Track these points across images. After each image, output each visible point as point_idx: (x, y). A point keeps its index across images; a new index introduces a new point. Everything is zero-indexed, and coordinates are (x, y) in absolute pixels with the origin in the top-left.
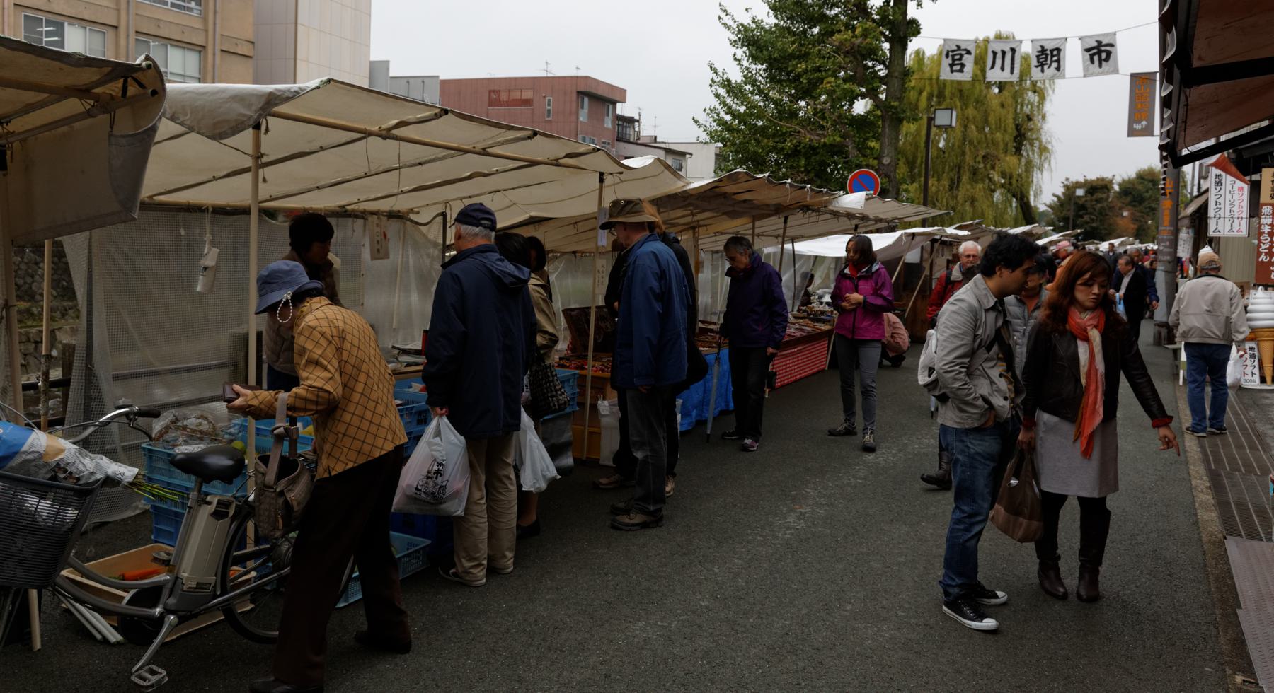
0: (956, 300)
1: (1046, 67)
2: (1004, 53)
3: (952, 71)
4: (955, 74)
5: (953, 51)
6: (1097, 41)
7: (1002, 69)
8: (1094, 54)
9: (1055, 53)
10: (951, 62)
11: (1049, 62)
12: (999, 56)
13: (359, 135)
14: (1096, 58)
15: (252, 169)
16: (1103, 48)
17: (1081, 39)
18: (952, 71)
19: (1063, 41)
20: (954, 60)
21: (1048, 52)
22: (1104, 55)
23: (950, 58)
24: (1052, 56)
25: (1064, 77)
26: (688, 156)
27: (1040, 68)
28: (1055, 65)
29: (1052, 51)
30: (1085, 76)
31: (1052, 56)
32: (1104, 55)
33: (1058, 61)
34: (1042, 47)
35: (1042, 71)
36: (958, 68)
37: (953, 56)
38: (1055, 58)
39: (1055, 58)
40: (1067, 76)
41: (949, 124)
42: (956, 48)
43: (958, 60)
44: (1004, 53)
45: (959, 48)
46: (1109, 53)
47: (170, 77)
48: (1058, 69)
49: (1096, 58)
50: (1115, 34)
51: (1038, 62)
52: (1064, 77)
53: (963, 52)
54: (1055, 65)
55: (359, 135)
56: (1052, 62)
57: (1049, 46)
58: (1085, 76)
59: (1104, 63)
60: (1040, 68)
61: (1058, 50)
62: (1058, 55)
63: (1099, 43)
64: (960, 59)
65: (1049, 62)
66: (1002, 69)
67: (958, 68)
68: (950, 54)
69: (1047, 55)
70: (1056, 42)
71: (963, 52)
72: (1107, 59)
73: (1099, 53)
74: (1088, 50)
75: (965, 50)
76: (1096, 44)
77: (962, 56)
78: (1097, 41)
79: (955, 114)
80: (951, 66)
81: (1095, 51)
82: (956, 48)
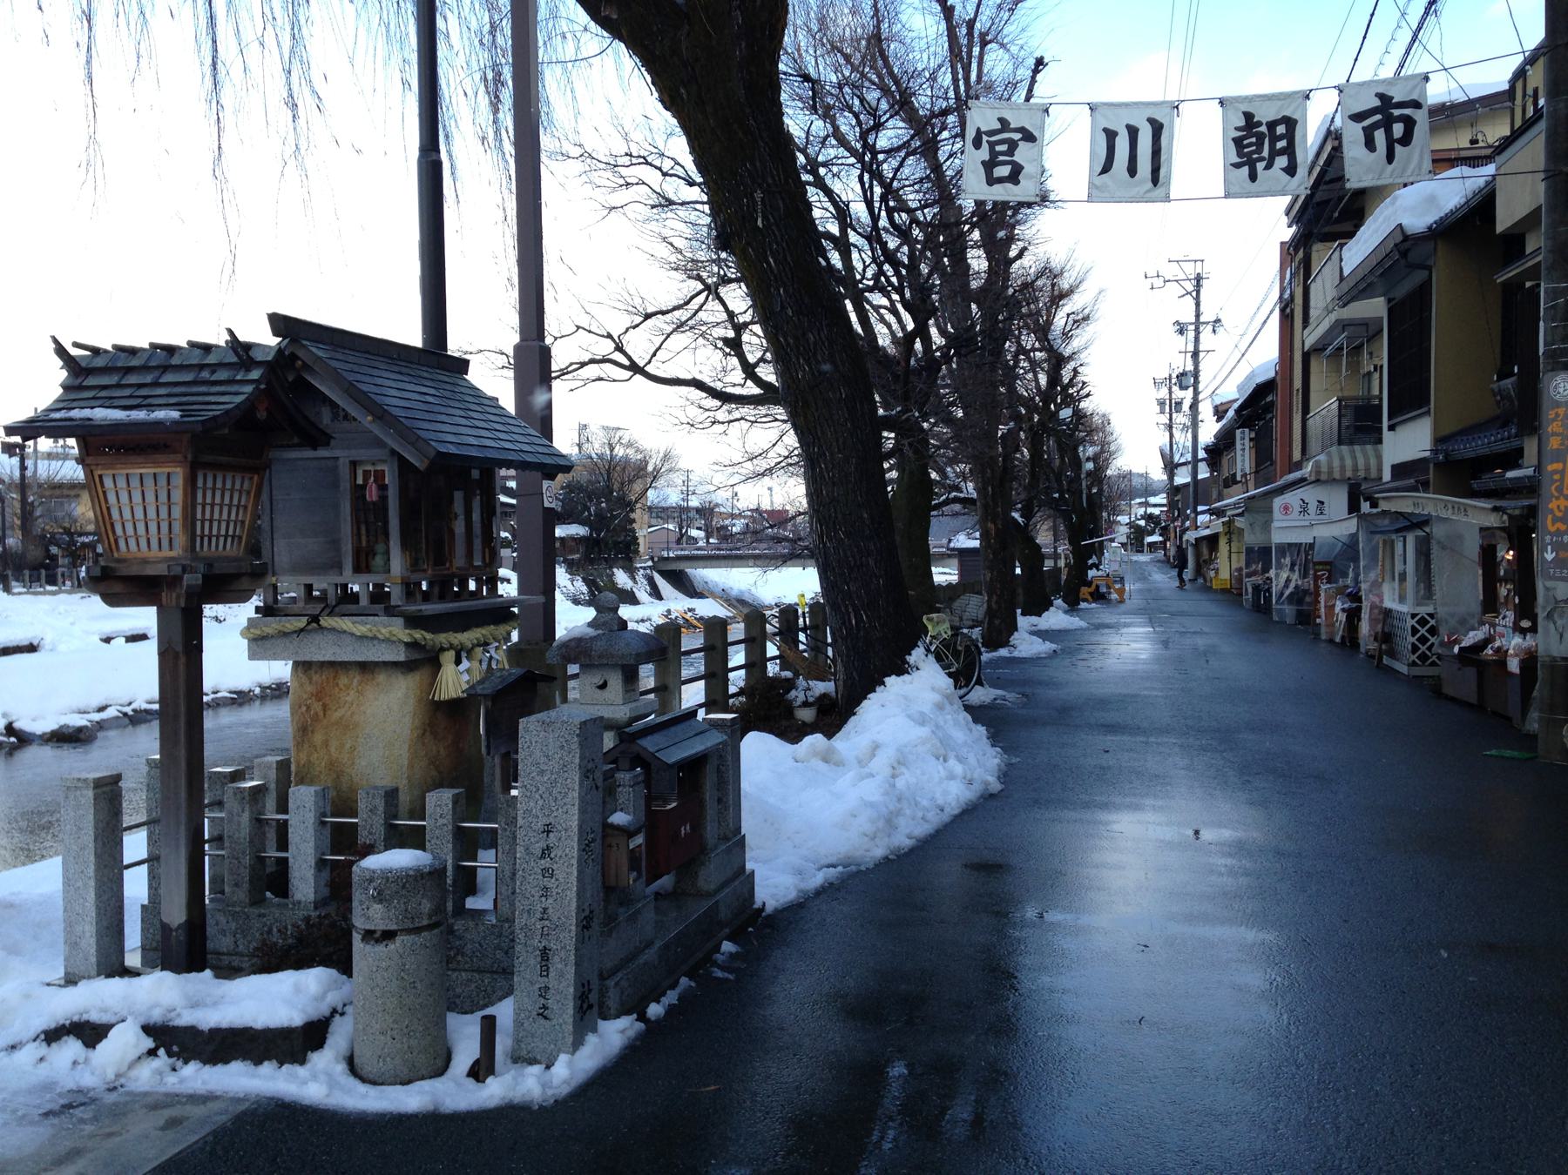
1: (1260, 166)
2: (1133, 132)
3: (991, 181)
4: (997, 187)
5: (991, 133)
6: (1377, 95)
7: (1132, 170)
8: (1375, 126)
9: (1281, 129)
10: (986, 157)
11: (1266, 153)
13: (627, 362)
14: (1380, 136)
16: (1397, 112)
18: (991, 181)
20: (994, 154)
21: (1263, 129)
22: (1398, 129)
23: (985, 146)
24: (1274, 139)
25: (1167, 199)
26: (541, 686)
27: (1246, 169)
28: (1282, 161)
29: (1272, 125)
31: (1274, 139)
32: (1398, 129)
34: (1248, 116)
35: (1253, 177)
36: (1003, 171)
37: (992, 145)
38: (1281, 144)
39: (1281, 144)
40: (1171, 198)
42: (998, 126)
43: (1002, 153)
44: (1133, 132)
49: (1380, 136)
50: (1427, 79)
51: (1240, 154)
53: (1017, 136)
54: (1282, 161)
55: (627, 362)
56: (1274, 153)
57: (1264, 115)
59: (1398, 148)
60: (1246, 169)
64: (1010, 152)
66: (1132, 170)
67: (1003, 171)
68: (985, 138)
69: (1261, 137)
71: (1017, 136)
73: (1387, 124)
75: (1022, 130)
76: (1377, 103)
77: (1013, 146)
78: (1377, 95)
80: (989, 166)
81: (1378, 117)
82: (998, 126)
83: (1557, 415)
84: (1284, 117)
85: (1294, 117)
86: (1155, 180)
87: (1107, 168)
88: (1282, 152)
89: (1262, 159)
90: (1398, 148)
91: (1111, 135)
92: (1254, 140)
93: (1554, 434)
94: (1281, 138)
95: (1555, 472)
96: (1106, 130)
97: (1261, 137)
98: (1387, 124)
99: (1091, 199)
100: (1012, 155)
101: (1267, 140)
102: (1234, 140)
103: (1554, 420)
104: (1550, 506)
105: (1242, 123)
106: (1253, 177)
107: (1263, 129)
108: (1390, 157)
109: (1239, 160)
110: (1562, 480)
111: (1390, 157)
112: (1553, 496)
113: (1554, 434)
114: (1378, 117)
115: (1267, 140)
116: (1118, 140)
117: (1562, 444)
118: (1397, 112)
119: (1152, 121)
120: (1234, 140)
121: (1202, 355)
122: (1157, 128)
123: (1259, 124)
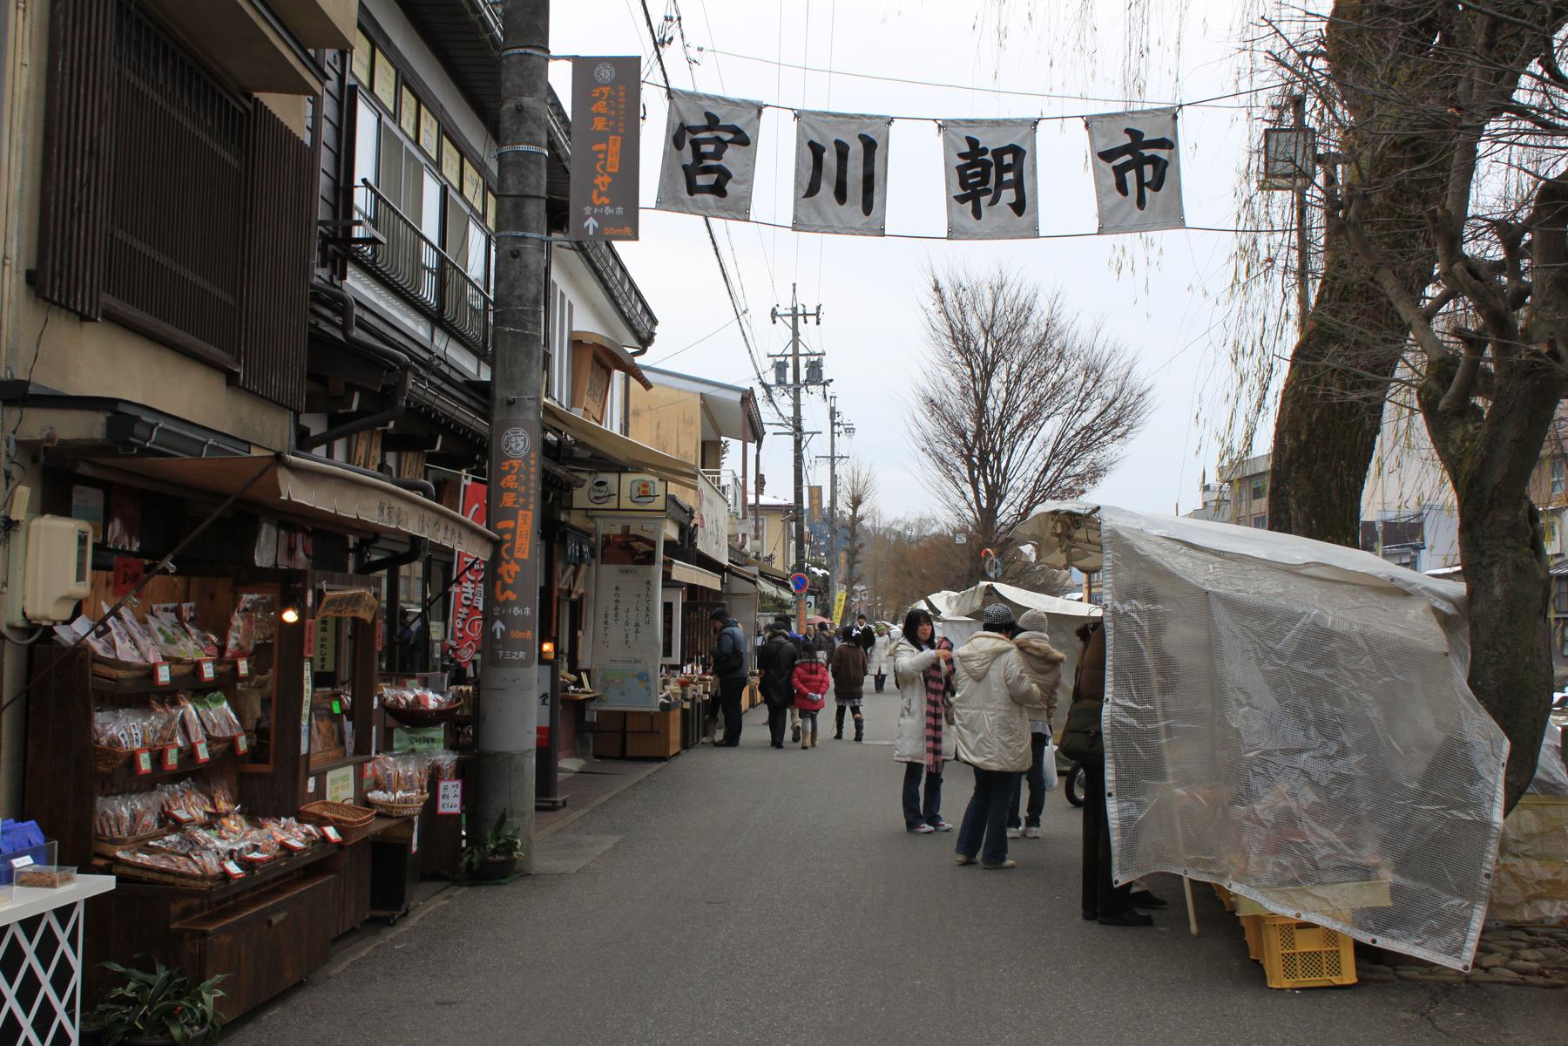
0: (227, 101)
2: (842, 150)
6: (1128, 131)
9: (1008, 159)
11: (992, 184)
12: (830, 158)
14: (1131, 176)
15: (1508, 265)
16: (1147, 153)
17: (798, 116)
19: (1028, 129)
20: (699, 156)
22: (1148, 170)
23: (688, 147)
24: (1002, 169)
27: (969, 205)
28: (1008, 195)
29: (998, 153)
30: (1101, 231)
32: (1148, 170)
33: (1018, 184)
34: (972, 142)
35: (977, 213)
36: (709, 180)
37: (696, 144)
39: (1009, 176)
41: (575, 506)
42: (705, 122)
44: (842, 150)
45: (712, 122)
46: (1161, 167)
47: (293, 535)
48: (1019, 207)
49: (1131, 176)
51: (963, 184)
52: (1033, 232)
53: (727, 136)
54: (1008, 195)
56: (1000, 185)
57: (990, 141)
58: (1101, 231)
60: (969, 205)
61: (1017, 152)
62: (1017, 166)
63: (1135, 134)
64: (718, 155)
65: (992, 184)
67: (709, 180)
70: (882, 182)
71: (727, 136)
72: (1157, 185)
73: (1138, 163)
74: (1106, 156)
76: (1127, 140)
77: (722, 145)
78: (1128, 131)
79: (1350, 233)
81: (1128, 157)
83: (602, 94)
84: (1011, 145)
85: (1024, 148)
86: (867, 207)
87: (813, 190)
88: (1008, 185)
89: (988, 192)
90: (1148, 192)
91: (817, 150)
92: (979, 169)
93: (599, 114)
94: (1008, 168)
95: (600, 151)
96: (812, 144)
97: (987, 165)
98: (1138, 163)
99: (797, 226)
100: (720, 158)
101: (993, 170)
102: (958, 168)
103: (599, 99)
104: (596, 182)
105: (966, 149)
106: (977, 213)
107: (988, 157)
108: (1141, 202)
109: (961, 192)
110: (606, 159)
111: (1141, 202)
112: (598, 173)
113: (599, 114)
114: (1128, 157)
115: (993, 170)
116: (826, 155)
117: (606, 126)
118: (1147, 153)
119: (862, 137)
120: (958, 168)
121: (836, 460)
122: (870, 145)
123: (985, 151)
